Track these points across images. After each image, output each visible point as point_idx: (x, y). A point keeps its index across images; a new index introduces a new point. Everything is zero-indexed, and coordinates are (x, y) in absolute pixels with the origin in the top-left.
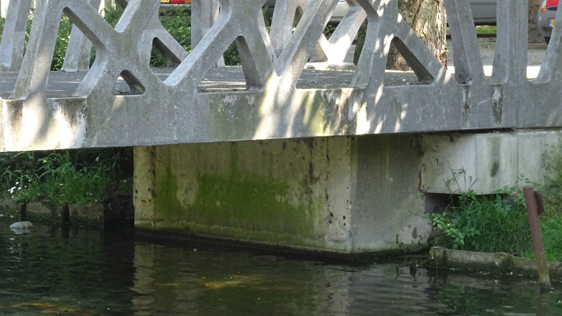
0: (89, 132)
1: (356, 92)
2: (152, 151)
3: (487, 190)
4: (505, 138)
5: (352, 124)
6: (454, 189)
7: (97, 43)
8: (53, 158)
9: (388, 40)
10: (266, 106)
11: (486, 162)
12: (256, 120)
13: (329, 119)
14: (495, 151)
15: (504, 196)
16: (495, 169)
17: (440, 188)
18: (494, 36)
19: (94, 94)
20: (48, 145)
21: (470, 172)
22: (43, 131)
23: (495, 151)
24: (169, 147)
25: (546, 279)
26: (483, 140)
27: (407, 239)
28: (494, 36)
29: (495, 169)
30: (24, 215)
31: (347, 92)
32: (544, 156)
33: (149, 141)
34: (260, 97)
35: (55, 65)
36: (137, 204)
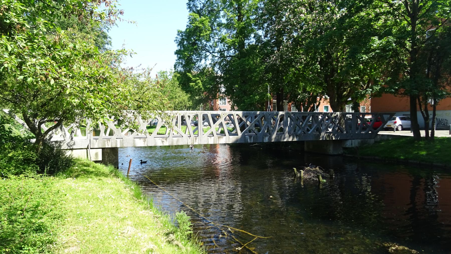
0: (299, 139)
1: (333, 134)
2: (307, 141)
3: (351, 147)
4: (353, 140)
5: (332, 138)
6: (346, 147)
7: (300, 128)
8: (385, 29)
9: (337, 128)
10: (321, 136)
11: (351, 143)
12: (320, 138)
13: (329, 138)
14: (352, 142)
15: (353, 148)
16: (352, 144)
17: (344, 146)
18: (157, 134)
19: (300, 134)
20: (294, 140)
21: (348, 145)
22: (293, 139)
23: (352, 142)
24: (309, 141)
25: (359, 158)
26: (350, 141)
27: (340, 153)
28: (157, 134)
29: (352, 144)
30: (291, 149)
31: (332, 134)
32: (358, 143)
33: (306, 140)
34: (321, 135)
35: (295, 131)
36: (305, 148)
